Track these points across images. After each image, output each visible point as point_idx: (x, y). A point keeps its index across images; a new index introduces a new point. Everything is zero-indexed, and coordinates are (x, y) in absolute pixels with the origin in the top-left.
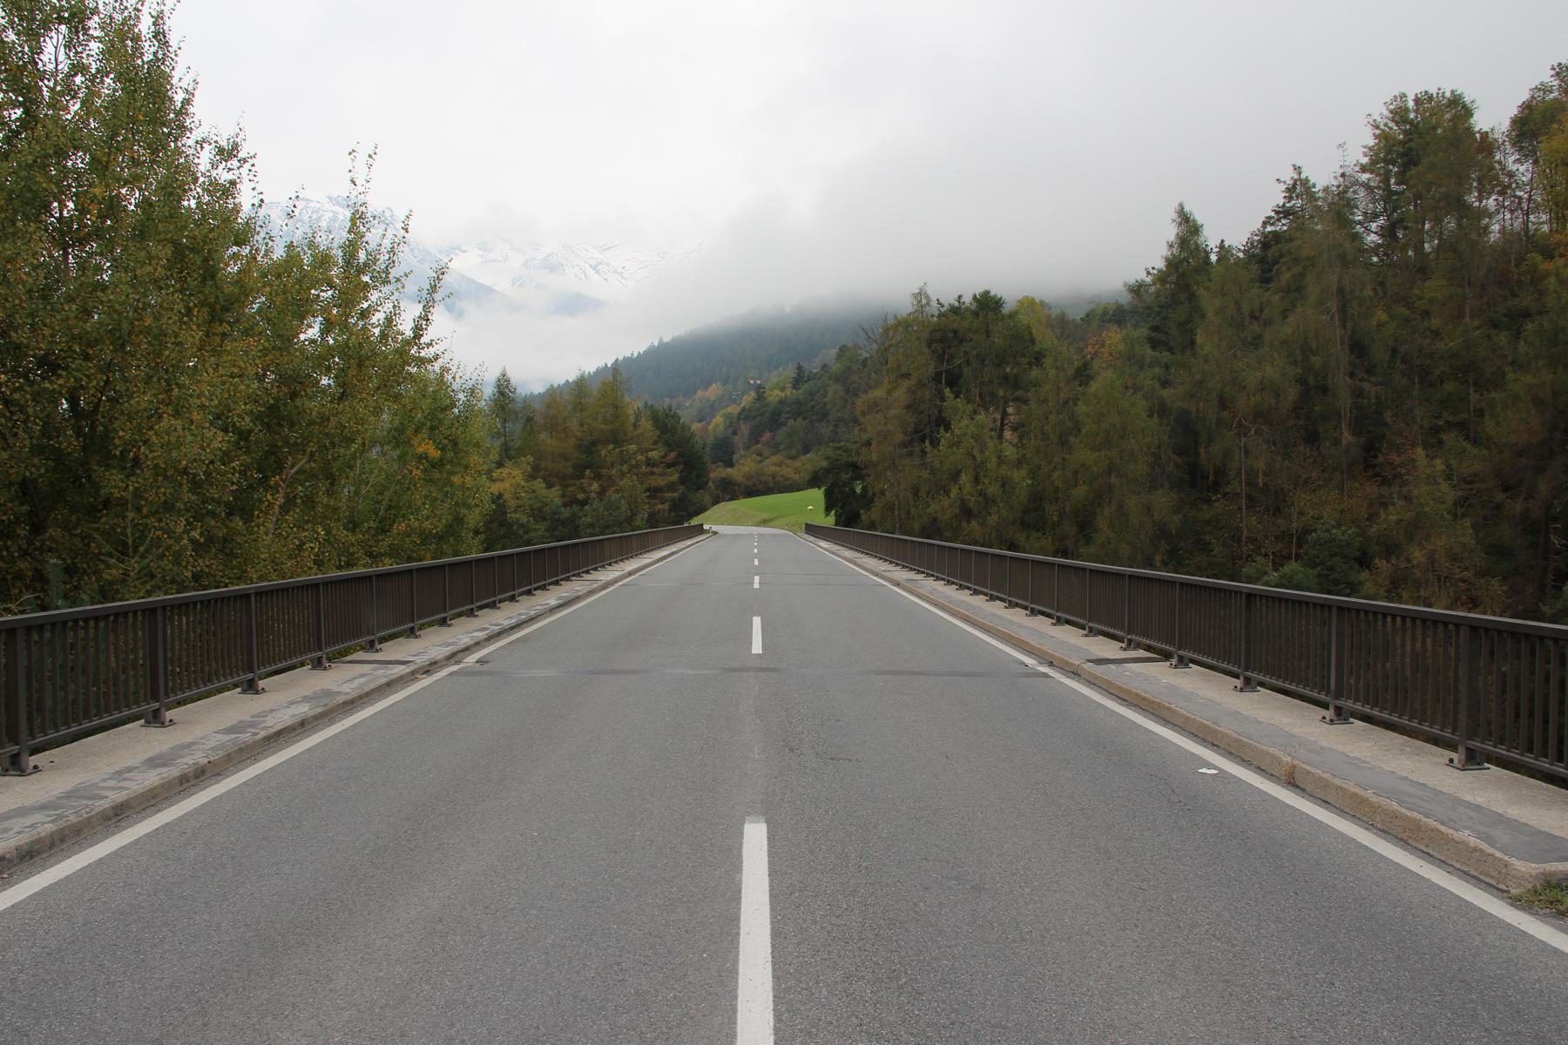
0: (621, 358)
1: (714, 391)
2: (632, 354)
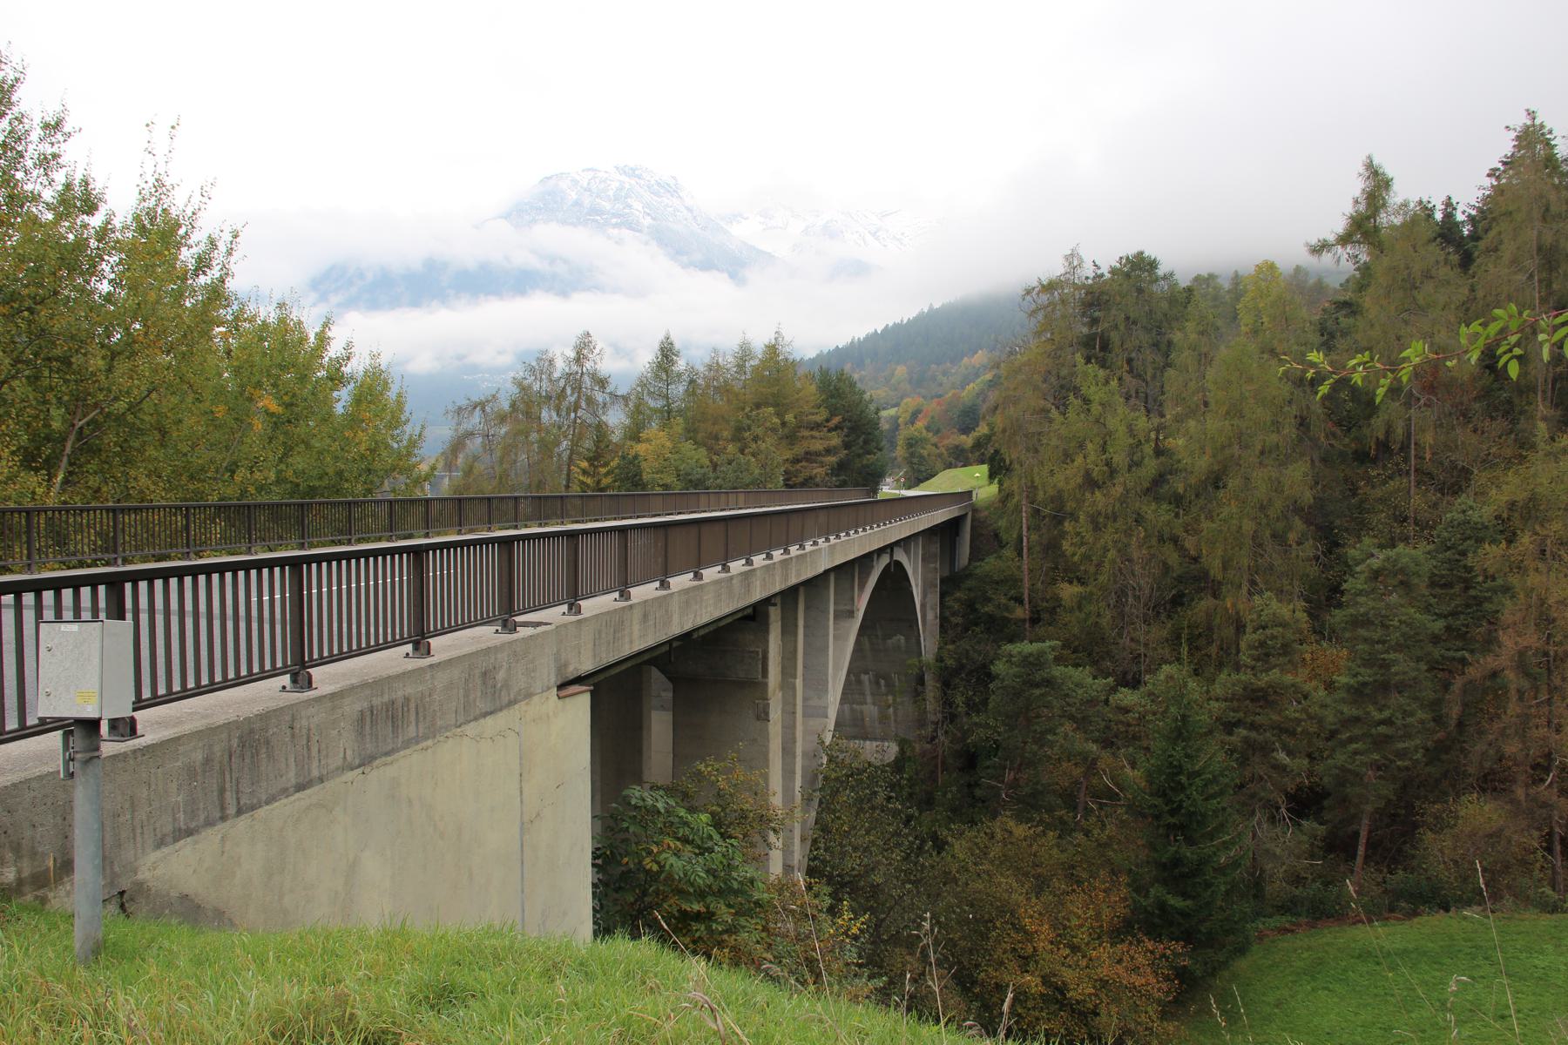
0: (891, 324)
1: (981, 357)
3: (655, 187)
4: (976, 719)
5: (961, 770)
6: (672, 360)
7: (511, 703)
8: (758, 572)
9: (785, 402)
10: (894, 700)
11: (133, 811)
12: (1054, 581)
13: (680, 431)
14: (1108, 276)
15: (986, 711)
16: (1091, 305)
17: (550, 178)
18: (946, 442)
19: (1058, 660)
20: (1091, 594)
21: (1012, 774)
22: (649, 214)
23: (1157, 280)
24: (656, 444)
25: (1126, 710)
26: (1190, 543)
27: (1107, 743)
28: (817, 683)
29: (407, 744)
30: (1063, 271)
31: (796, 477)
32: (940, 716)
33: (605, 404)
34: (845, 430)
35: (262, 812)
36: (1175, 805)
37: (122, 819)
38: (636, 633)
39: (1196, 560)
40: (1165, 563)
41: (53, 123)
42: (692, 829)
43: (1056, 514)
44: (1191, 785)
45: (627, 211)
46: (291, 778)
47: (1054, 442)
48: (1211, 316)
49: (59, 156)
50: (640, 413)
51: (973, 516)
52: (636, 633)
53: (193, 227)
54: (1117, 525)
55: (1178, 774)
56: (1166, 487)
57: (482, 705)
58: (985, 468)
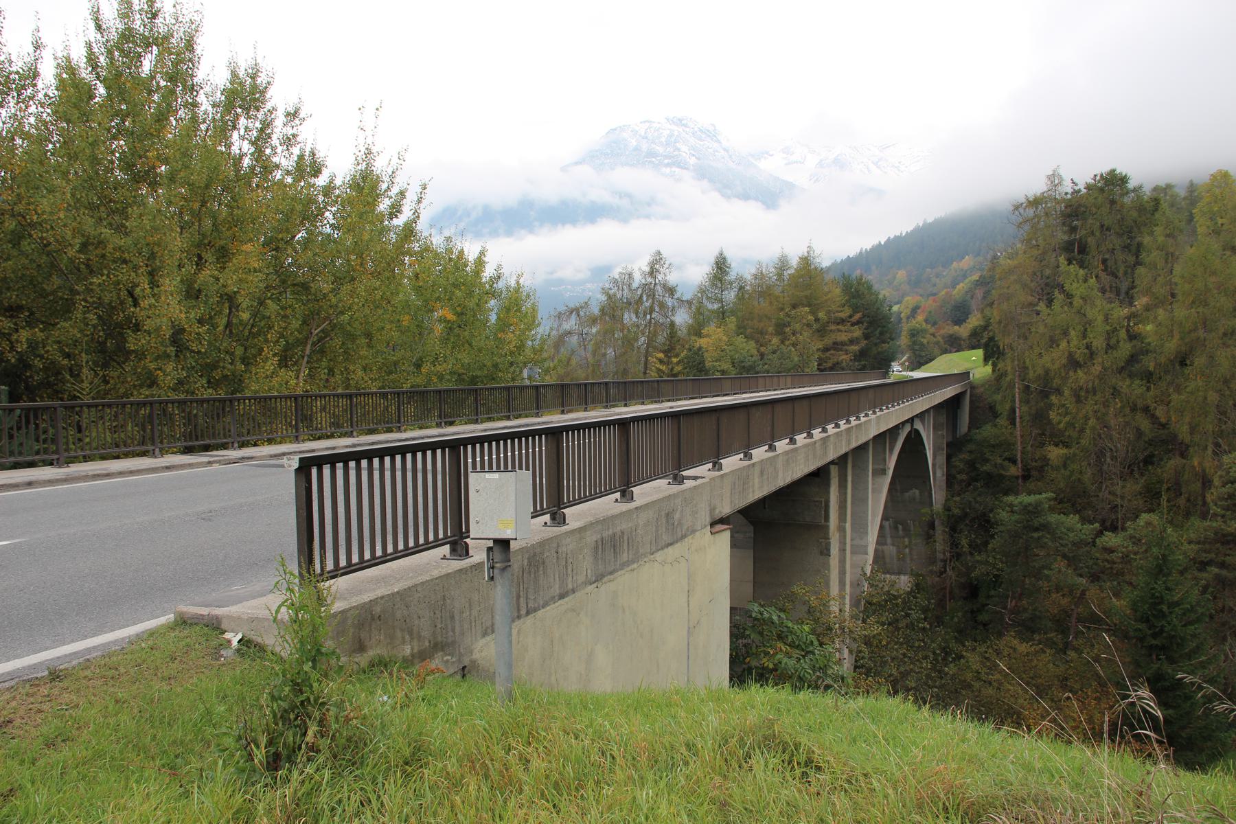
0: (892, 237)
1: (967, 262)
2: (901, 234)
3: (699, 133)
4: (978, 558)
5: (965, 599)
6: (725, 271)
7: (684, 537)
8: (832, 438)
9: (816, 302)
10: (910, 542)
11: (470, 610)
12: (1042, 445)
13: (734, 328)
14: (1084, 191)
15: (986, 551)
16: (1069, 216)
17: (615, 129)
18: (942, 332)
19: (1051, 509)
20: (1075, 455)
21: (1014, 601)
22: (693, 155)
23: (1127, 193)
24: (714, 339)
25: (1110, 551)
26: (1160, 412)
27: (1095, 578)
28: (860, 527)
29: (623, 566)
30: (1045, 189)
31: (826, 362)
32: (948, 555)
33: (674, 308)
34: (865, 324)
35: (540, 613)
36: (1157, 630)
37: (464, 615)
38: (757, 486)
39: (1163, 426)
40: (1138, 429)
41: (292, 112)
42: (798, 636)
43: (1046, 389)
44: (1171, 613)
45: (676, 153)
46: (556, 590)
47: (1042, 329)
48: (1177, 221)
49: (297, 135)
50: (700, 314)
51: (971, 392)
52: (757, 486)
53: (393, 183)
54: (1096, 398)
55: (1159, 603)
56: (1137, 366)
57: (666, 538)
58: (980, 353)
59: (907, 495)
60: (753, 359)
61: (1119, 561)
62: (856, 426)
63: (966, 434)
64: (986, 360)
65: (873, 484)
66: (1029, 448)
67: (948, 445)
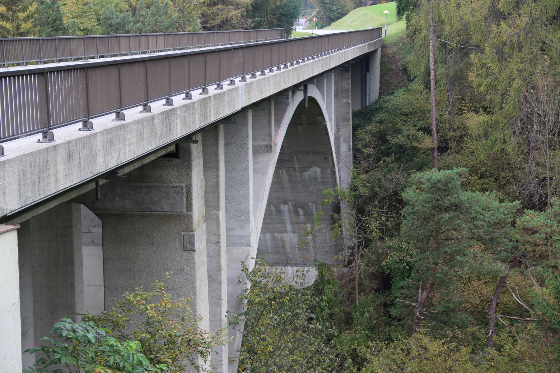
4: (389, 243)
10: (312, 228)
12: (460, 112)
19: (465, 185)
21: (425, 293)
31: (213, 19)
32: (356, 241)
59: (306, 174)
60: (122, 15)
61: (541, 242)
62: (216, 96)
63: (377, 102)
64: (400, 13)
65: (254, 163)
66: (447, 115)
67: (354, 115)
